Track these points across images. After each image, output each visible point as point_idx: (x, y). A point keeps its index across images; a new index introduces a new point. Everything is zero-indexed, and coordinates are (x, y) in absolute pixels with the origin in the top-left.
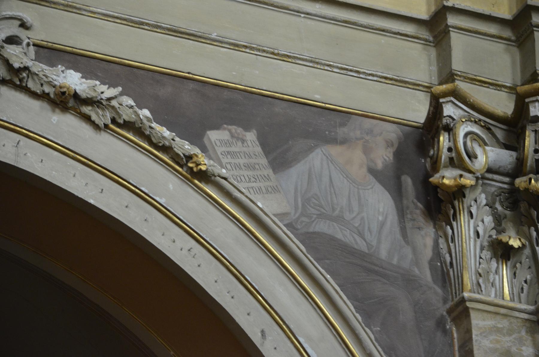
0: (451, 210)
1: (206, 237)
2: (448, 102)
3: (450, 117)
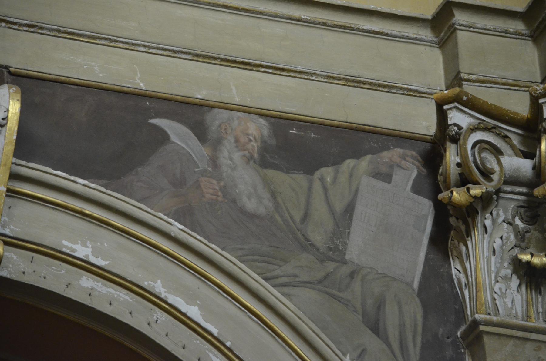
0: (527, 238)
1: (70, 251)
2: (451, 109)
3: (455, 125)
